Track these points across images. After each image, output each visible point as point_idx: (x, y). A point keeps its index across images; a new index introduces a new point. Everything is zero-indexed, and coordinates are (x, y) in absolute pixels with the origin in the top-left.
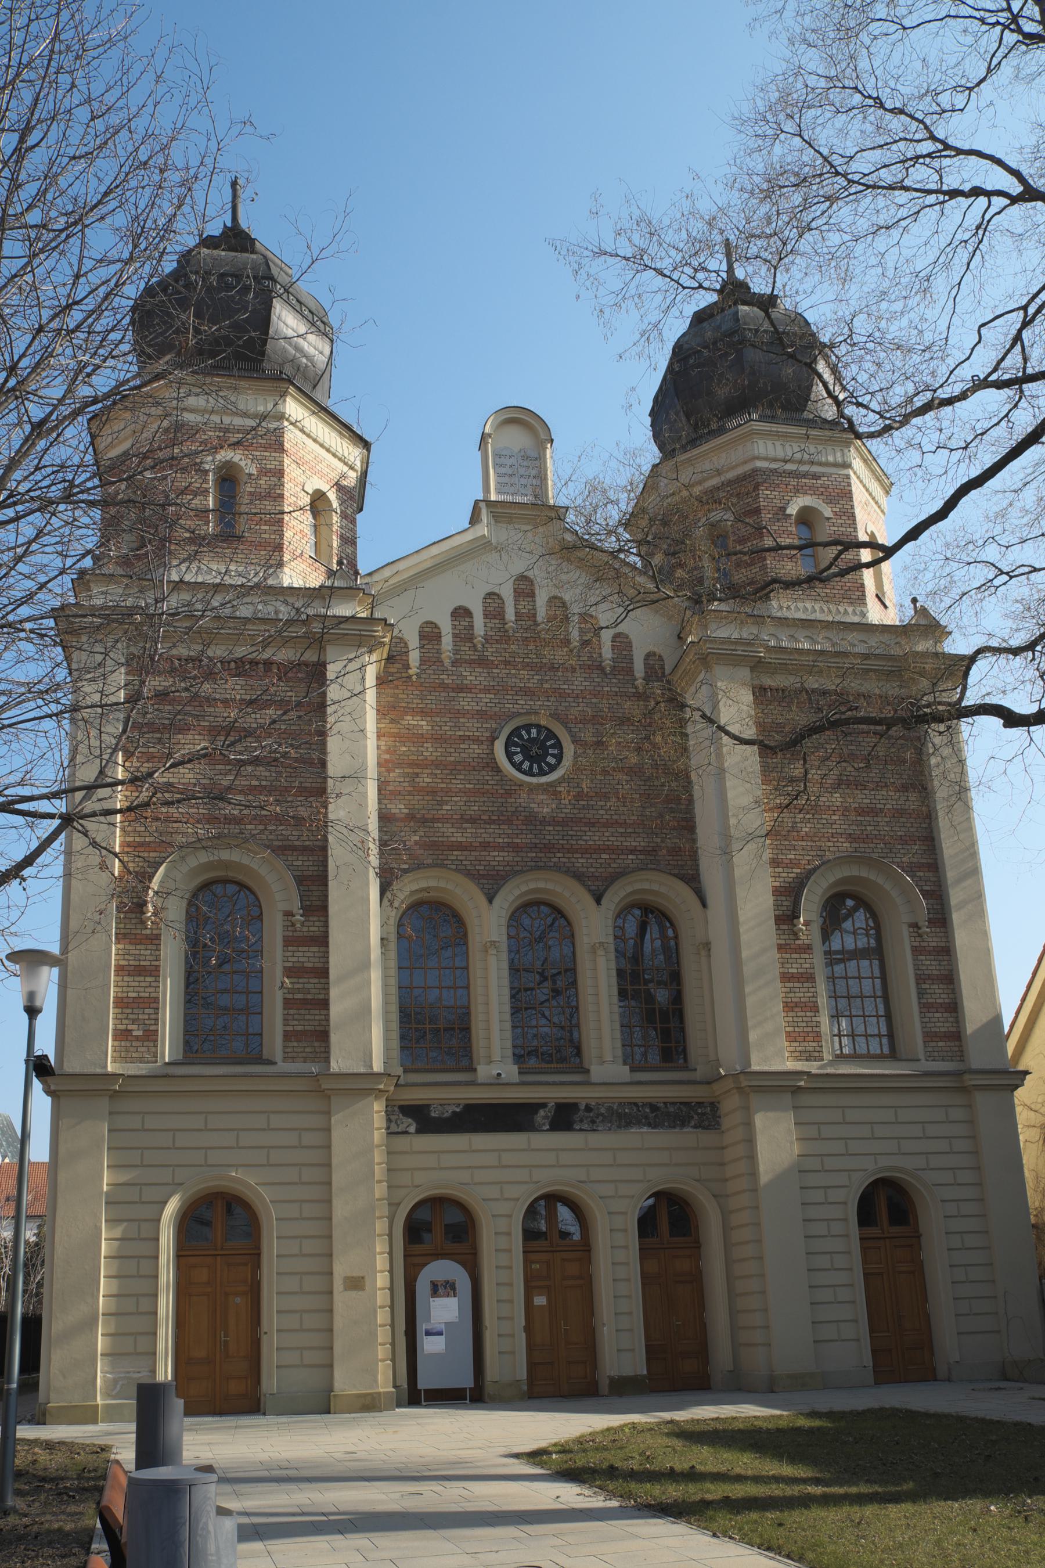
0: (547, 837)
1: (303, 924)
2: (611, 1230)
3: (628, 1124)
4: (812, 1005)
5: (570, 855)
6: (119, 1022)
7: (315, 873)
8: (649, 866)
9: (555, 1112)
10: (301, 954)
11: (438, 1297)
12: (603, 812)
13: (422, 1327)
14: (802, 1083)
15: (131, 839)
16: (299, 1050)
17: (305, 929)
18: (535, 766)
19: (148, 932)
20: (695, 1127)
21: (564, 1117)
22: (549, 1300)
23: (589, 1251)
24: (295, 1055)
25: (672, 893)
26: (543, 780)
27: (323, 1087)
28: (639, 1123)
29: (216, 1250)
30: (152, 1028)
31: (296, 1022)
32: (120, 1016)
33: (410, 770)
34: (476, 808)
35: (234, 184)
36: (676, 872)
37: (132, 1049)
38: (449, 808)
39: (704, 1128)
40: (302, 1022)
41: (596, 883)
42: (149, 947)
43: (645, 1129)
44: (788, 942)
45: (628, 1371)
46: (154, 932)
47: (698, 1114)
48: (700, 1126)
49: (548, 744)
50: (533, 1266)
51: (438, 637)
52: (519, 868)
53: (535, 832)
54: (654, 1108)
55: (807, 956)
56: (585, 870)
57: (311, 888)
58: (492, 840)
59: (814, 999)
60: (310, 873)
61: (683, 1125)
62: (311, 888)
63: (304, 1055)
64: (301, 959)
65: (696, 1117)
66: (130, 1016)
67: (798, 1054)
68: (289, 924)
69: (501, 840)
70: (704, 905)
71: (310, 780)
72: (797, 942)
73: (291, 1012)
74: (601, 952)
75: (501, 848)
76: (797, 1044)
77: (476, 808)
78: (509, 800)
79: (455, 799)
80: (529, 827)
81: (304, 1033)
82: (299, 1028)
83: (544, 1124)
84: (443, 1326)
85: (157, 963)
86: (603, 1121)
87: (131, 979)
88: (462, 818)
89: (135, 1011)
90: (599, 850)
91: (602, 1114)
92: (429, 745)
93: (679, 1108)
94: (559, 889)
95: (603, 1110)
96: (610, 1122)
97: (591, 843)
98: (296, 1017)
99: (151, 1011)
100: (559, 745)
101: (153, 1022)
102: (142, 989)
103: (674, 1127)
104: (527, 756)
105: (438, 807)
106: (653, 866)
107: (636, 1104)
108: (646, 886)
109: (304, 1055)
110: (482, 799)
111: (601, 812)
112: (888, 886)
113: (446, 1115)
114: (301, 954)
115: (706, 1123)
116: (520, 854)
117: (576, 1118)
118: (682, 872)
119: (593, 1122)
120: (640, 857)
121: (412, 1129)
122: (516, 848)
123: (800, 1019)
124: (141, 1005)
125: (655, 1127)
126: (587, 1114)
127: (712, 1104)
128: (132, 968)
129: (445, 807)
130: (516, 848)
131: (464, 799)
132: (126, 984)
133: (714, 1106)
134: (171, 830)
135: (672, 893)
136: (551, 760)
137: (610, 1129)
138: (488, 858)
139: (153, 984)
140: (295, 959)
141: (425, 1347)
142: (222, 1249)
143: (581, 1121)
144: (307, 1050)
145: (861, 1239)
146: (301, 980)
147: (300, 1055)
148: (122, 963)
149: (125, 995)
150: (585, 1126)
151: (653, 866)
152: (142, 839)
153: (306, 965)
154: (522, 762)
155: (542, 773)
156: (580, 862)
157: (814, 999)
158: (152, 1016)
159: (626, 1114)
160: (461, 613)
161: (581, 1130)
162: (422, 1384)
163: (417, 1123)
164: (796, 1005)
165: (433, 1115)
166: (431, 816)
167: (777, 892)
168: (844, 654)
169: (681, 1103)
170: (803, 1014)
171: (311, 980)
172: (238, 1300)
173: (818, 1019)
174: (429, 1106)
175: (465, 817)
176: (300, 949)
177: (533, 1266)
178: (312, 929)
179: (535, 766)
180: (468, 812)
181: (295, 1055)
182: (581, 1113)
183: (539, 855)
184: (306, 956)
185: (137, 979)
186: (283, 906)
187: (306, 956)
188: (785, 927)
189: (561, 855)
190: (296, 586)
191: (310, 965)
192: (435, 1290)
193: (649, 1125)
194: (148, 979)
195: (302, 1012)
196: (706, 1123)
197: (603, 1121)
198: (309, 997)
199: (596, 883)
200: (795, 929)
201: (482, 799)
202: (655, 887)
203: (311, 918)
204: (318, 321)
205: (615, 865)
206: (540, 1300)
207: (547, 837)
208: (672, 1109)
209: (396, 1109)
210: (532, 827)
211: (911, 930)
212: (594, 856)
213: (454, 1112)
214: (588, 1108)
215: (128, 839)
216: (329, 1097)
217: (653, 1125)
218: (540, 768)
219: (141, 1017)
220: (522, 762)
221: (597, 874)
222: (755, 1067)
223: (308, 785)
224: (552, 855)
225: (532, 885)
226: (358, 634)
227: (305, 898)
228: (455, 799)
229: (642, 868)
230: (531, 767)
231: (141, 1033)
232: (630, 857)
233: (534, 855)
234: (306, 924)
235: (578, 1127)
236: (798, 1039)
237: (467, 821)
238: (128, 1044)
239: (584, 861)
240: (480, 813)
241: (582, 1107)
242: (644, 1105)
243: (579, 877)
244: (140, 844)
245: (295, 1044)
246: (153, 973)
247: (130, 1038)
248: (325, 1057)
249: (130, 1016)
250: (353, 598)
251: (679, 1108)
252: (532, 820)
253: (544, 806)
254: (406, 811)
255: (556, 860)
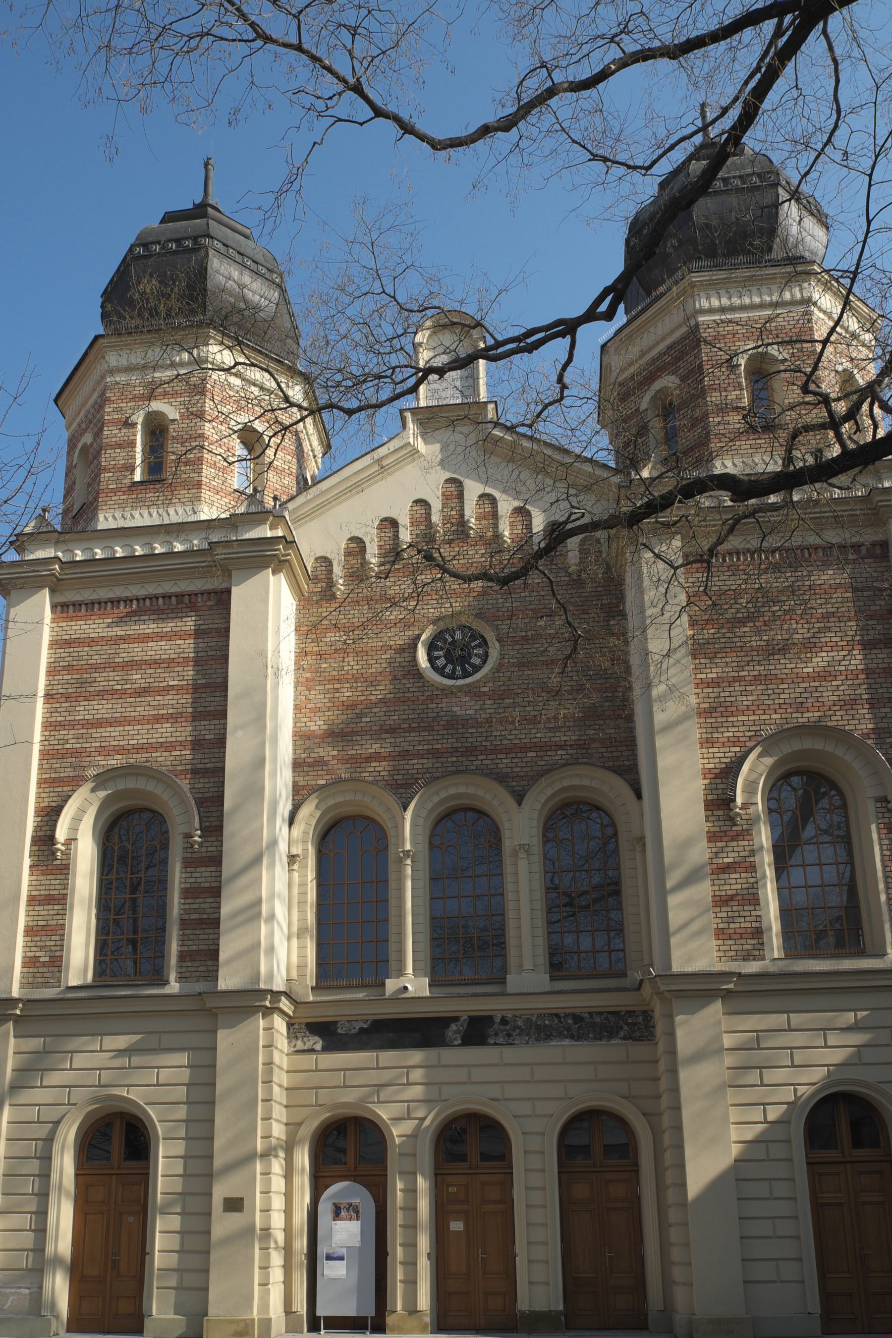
0: (470, 740)
1: (201, 844)
2: (525, 1152)
3: (549, 1037)
4: (751, 897)
5: (494, 756)
6: (28, 949)
7: (215, 794)
8: (580, 761)
9: (468, 1025)
10: (198, 875)
11: (340, 1220)
12: (531, 708)
13: (322, 1249)
14: (731, 986)
15: (48, 776)
16: (193, 969)
17: (204, 849)
18: (458, 668)
19: (58, 862)
20: (625, 1038)
21: (477, 1031)
22: (466, 1225)
23: (637, 1171)
24: (188, 974)
25: (609, 787)
26: (469, 680)
27: (208, 1005)
28: (561, 1036)
29: (112, 1169)
30: (58, 954)
31: (191, 943)
32: (29, 944)
33: (331, 686)
34: (396, 717)
35: (206, 165)
36: (611, 764)
37: (38, 975)
38: (368, 719)
39: (635, 1039)
40: (196, 942)
41: (521, 783)
42: (59, 877)
43: (567, 1042)
44: (723, 829)
45: (540, 1306)
46: (64, 862)
47: (628, 1024)
48: (630, 1038)
49: (473, 644)
50: (450, 1189)
51: (363, 549)
52: (439, 774)
53: (457, 736)
54: (577, 1018)
55: (746, 843)
56: (509, 770)
57: (211, 809)
58: (411, 748)
59: (754, 891)
60: (211, 795)
61: (610, 1036)
62: (211, 809)
63: (197, 974)
64: (198, 880)
65: (626, 1027)
66: (39, 944)
67: (733, 953)
68: (189, 845)
69: (420, 748)
70: (639, 796)
71: (215, 704)
72: (734, 828)
73: (187, 932)
74: (522, 855)
75: (419, 756)
76: (732, 942)
77: (396, 717)
78: (430, 706)
79: (375, 710)
80: (450, 732)
81: (198, 952)
82: (194, 948)
83: (456, 1039)
84: (344, 1251)
85: (64, 892)
86: (520, 1034)
87: (41, 908)
88: (381, 729)
89: (44, 938)
90: (525, 748)
91: (519, 1027)
92: (351, 659)
93: (607, 1018)
94: (480, 793)
95: (520, 1023)
96: (528, 1035)
97: (516, 742)
98: (191, 937)
99: (58, 938)
100: (484, 643)
101: (58, 948)
102: (50, 918)
103: (600, 1039)
104: (448, 657)
105: (359, 720)
106: (585, 760)
107: (557, 1015)
108: (576, 782)
109: (197, 974)
110: (403, 708)
111: (528, 709)
112: (848, 758)
113: (353, 1031)
114: (198, 875)
115: (638, 1034)
116: (440, 760)
117: (491, 1031)
118: (617, 764)
119: (509, 1035)
120: (570, 752)
121: (318, 1047)
122: (435, 754)
123: (737, 914)
124: (49, 933)
125: (579, 1039)
126: (503, 1027)
127: (645, 1012)
128: (43, 897)
129: (364, 720)
130: (435, 754)
131: (384, 709)
132: (36, 913)
133: (647, 1015)
134: (85, 764)
135: (609, 787)
136: (476, 661)
137: (527, 1043)
138: (406, 767)
139: (60, 912)
140: (192, 880)
141: (325, 1273)
142: (119, 1168)
143: (496, 1035)
144: (201, 969)
145: (808, 1163)
146: (197, 901)
147: (193, 974)
148: (34, 893)
149: (35, 923)
150: (501, 1040)
151: (585, 760)
152: (57, 775)
153: (203, 885)
154: (445, 666)
155: (466, 675)
156: (504, 763)
157: (754, 891)
158: (58, 943)
159: (546, 1026)
160: (390, 524)
161: (495, 1044)
162: (322, 1311)
163: (323, 1041)
164: (732, 898)
165: (340, 1031)
166: (350, 730)
167: (705, 773)
168: (566, 452)
169: (609, 1013)
170: (740, 908)
171: (208, 900)
172: (131, 1219)
173: (758, 913)
174: (335, 1023)
175: (385, 727)
176: (198, 869)
177: (450, 1189)
178: (210, 849)
179: (458, 668)
180: (388, 723)
181: (188, 974)
182: (496, 1026)
183: (460, 759)
184: (202, 876)
185: (46, 907)
186: (183, 829)
187: (202, 876)
188: (721, 813)
189: (484, 757)
190: (214, 517)
191: (207, 885)
192: (337, 1214)
193: (572, 1037)
194: (56, 907)
195: (198, 932)
196: (638, 1034)
197: (520, 1034)
198: (205, 916)
199: (521, 783)
200: (731, 814)
201: (403, 708)
202: (586, 782)
203: (210, 839)
204: (267, 270)
205: (543, 763)
206: (457, 1226)
207: (470, 740)
208: (598, 1020)
209: (303, 1026)
210: (454, 731)
211: (879, 805)
212: (519, 755)
213: (361, 1029)
214: (504, 1021)
215: (44, 776)
216: (216, 1015)
217: (577, 1037)
218: (464, 670)
219: (48, 943)
220: (445, 666)
221: (522, 774)
222: (676, 968)
223: (212, 708)
224: (474, 758)
225: (452, 791)
226: (266, 556)
227: (204, 819)
228: (375, 710)
229: (575, 762)
230: (454, 670)
231: (47, 959)
232: (559, 752)
233: (455, 759)
234: (205, 844)
235: (492, 1041)
236: (733, 936)
237: (387, 731)
238: (35, 970)
239: (509, 761)
240: (400, 722)
241: (498, 1020)
242: (566, 1016)
243: (502, 778)
244: (54, 780)
245: (189, 964)
246: (61, 902)
247: (37, 964)
248: (213, 975)
249: (39, 944)
250: (263, 522)
251: (607, 1018)
252: (454, 724)
253: (465, 708)
254: (325, 727)
255: (478, 763)
